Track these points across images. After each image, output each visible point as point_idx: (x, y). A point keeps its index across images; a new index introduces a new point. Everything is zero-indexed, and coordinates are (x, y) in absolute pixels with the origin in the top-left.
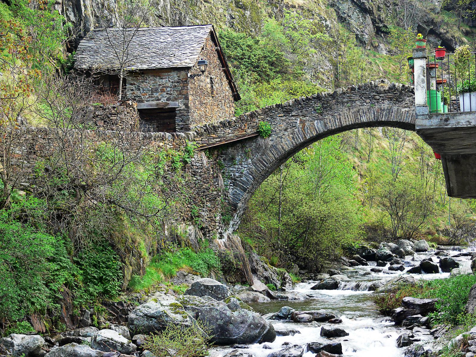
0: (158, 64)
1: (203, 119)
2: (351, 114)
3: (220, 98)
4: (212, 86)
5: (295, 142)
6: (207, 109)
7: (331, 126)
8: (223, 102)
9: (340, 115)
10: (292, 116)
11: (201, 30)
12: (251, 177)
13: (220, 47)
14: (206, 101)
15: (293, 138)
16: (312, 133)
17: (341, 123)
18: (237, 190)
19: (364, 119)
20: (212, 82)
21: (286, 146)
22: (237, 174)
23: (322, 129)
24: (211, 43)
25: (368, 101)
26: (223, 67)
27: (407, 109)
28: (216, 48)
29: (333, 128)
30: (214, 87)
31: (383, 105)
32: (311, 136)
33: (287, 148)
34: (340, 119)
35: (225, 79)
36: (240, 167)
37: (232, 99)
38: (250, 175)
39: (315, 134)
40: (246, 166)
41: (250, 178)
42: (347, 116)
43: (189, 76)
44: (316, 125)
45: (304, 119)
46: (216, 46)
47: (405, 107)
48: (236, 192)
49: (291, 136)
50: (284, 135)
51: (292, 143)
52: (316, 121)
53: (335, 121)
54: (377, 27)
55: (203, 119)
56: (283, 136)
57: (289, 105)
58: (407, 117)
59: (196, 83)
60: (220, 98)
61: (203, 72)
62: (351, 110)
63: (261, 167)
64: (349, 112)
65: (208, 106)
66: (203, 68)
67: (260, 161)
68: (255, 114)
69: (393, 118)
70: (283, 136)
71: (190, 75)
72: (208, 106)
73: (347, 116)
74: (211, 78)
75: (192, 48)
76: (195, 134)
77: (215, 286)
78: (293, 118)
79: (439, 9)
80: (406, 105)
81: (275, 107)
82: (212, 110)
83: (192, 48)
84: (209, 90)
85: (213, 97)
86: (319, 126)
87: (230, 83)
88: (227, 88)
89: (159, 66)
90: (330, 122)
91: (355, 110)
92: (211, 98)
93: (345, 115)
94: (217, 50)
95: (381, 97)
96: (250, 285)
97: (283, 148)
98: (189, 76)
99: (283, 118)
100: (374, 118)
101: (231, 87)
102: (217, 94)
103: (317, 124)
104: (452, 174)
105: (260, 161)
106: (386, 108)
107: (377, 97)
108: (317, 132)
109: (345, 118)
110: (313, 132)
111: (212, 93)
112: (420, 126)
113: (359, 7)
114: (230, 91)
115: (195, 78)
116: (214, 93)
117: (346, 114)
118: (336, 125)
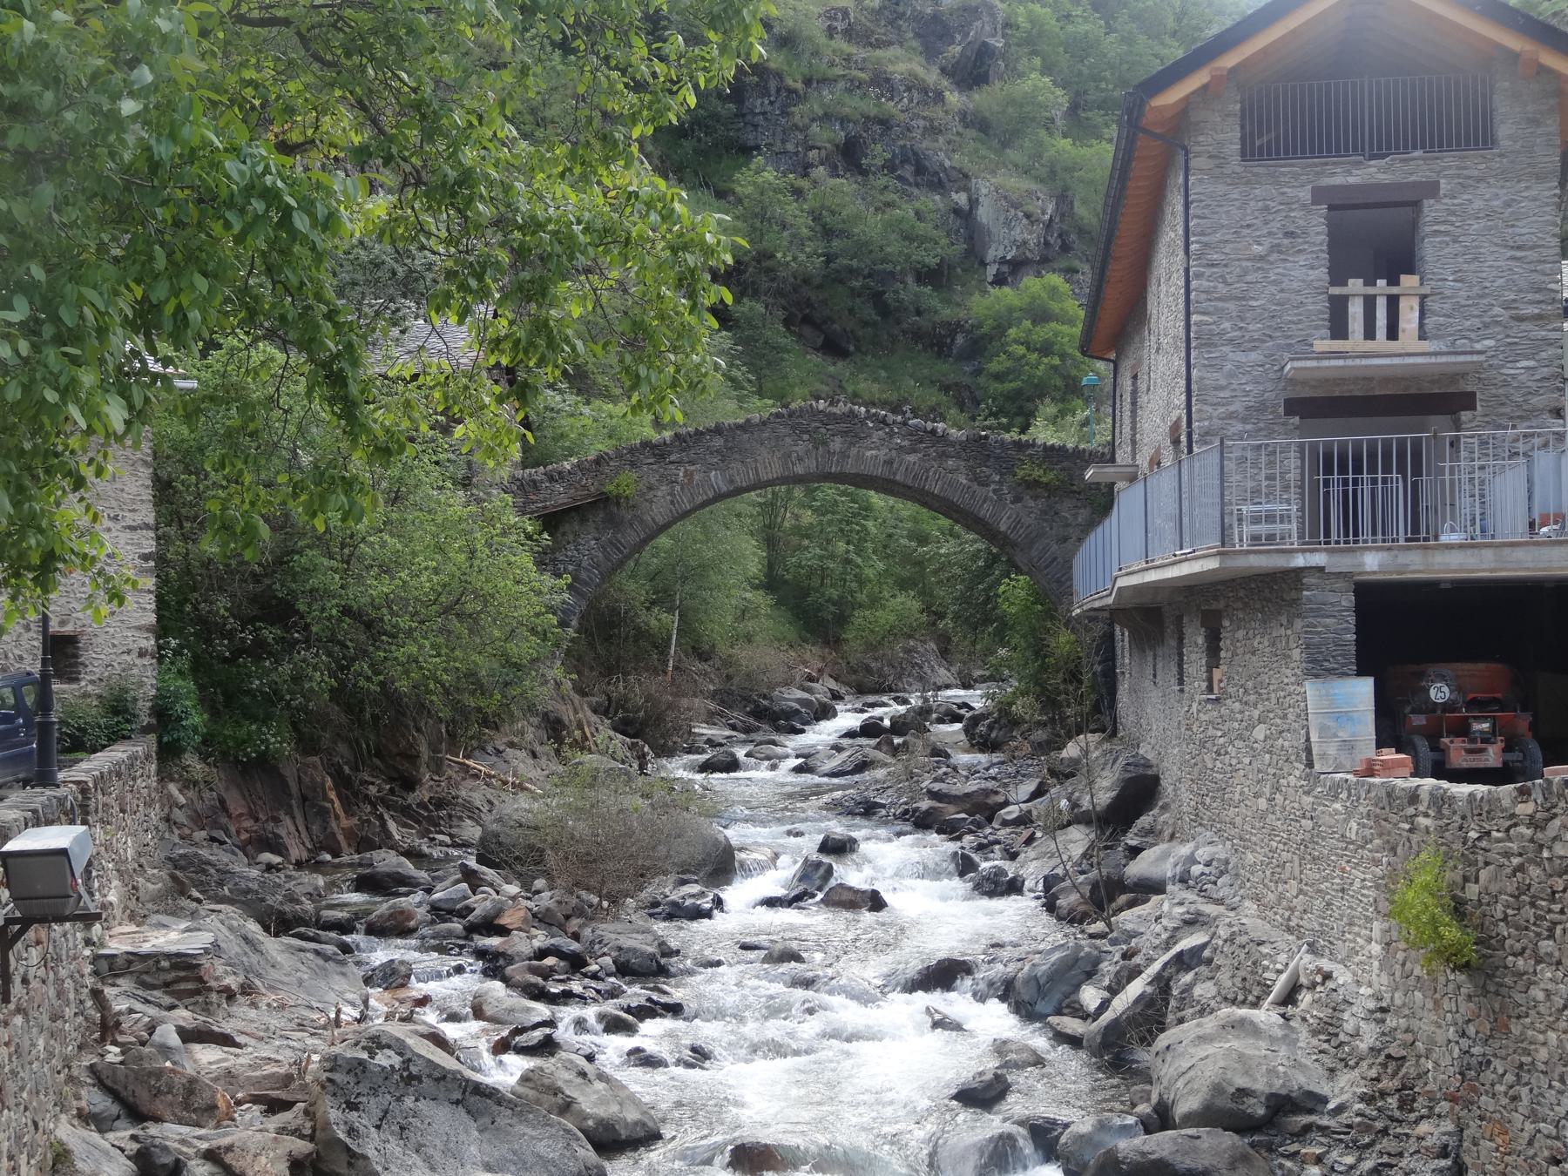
15: (672, 502)
25: (806, 437)
39: (711, 494)
69: (850, 467)
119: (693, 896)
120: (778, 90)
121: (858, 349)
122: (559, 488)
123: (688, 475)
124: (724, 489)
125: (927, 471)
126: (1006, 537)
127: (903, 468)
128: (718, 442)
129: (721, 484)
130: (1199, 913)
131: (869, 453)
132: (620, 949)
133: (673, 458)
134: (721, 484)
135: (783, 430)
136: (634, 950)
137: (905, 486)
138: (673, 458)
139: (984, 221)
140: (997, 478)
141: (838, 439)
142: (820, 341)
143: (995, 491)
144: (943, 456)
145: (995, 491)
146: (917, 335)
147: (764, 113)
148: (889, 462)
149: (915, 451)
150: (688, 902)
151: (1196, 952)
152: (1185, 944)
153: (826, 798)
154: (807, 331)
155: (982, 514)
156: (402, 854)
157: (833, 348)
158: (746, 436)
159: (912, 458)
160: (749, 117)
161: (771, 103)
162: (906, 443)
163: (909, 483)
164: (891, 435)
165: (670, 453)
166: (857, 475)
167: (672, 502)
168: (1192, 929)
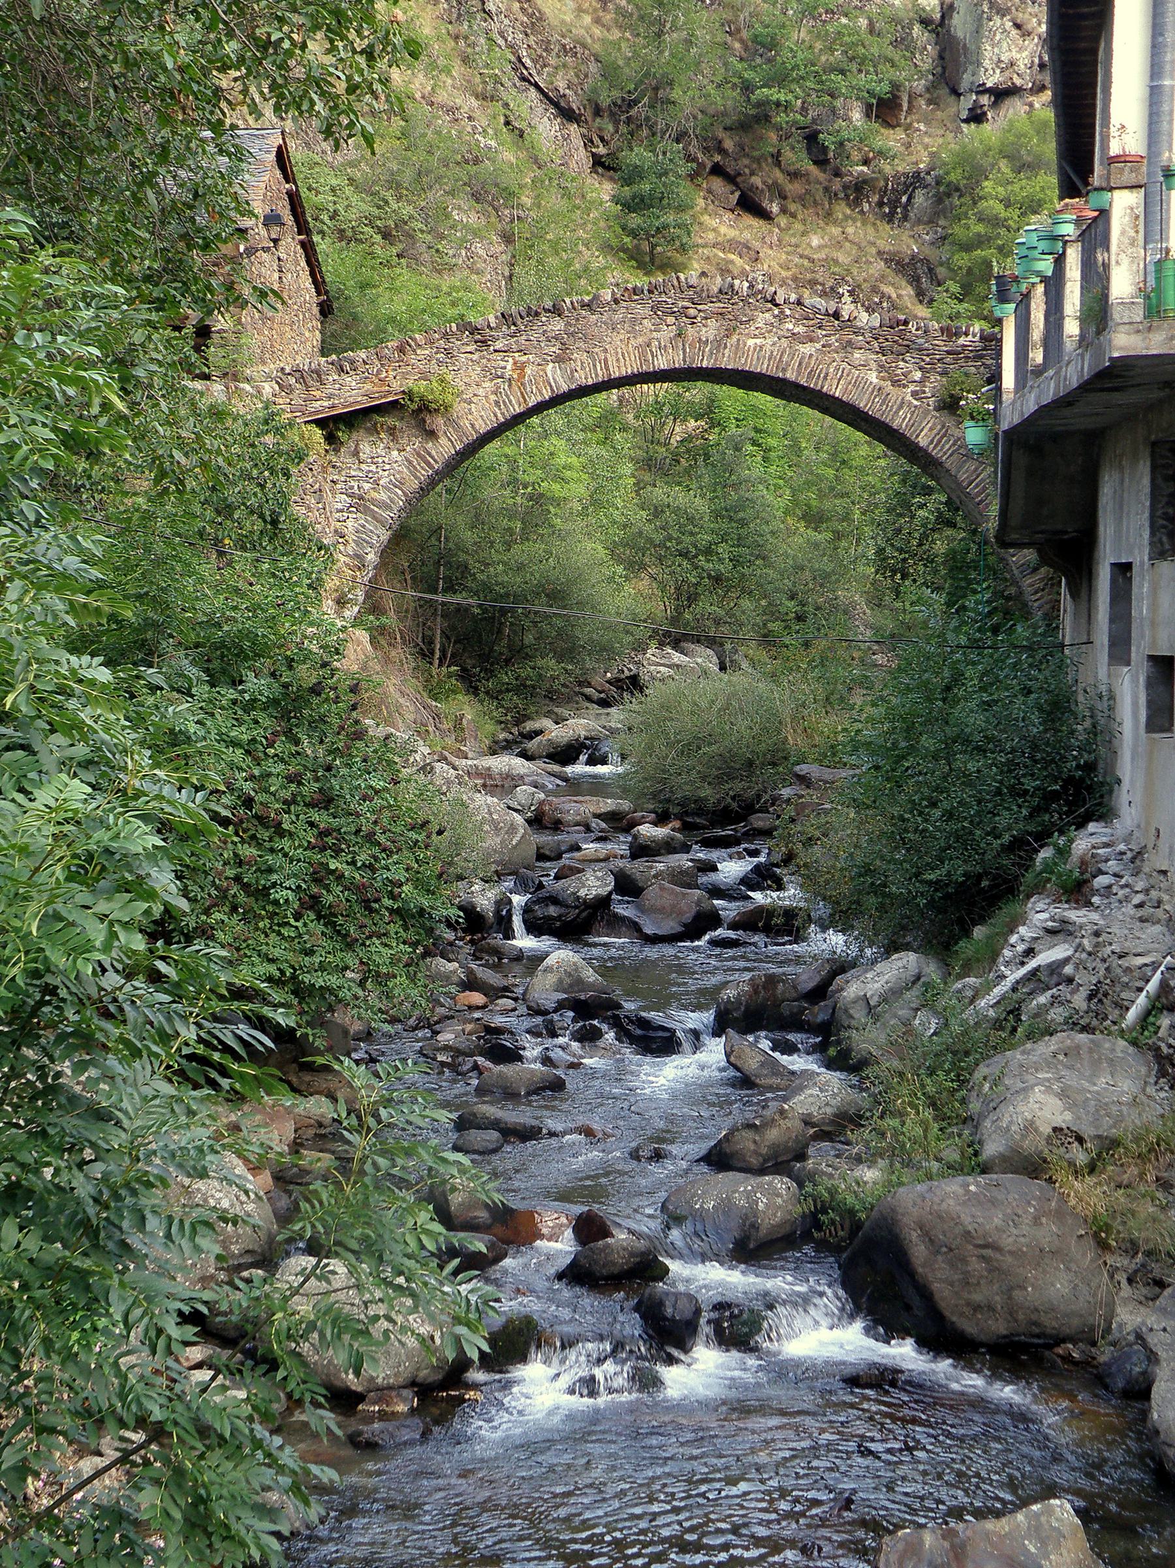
7: (585, 378)
9: (606, 351)
15: (497, 403)
17: (607, 369)
19: (662, 363)
22: (367, 486)
27: (758, 341)
29: (590, 382)
32: (540, 399)
34: (606, 360)
35: (303, 263)
36: (373, 468)
39: (547, 395)
41: (396, 494)
45: (524, 358)
47: (755, 337)
49: (493, 397)
54: (593, 155)
56: (475, 399)
62: (632, 341)
63: (424, 473)
67: (419, 455)
69: (727, 361)
70: (475, 399)
76: (277, 387)
78: (499, 356)
86: (558, 379)
87: (313, 274)
91: (640, 340)
97: (473, 425)
99: (475, 357)
101: (315, 282)
103: (554, 372)
104: (1018, 477)
105: (419, 455)
106: (711, 338)
107: (692, 312)
112: (1121, 348)
113: (556, 105)
121: (784, 210)
123: (520, 367)
124: (564, 388)
126: (924, 451)
127: (797, 360)
129: (561, 381)
130: (1064, 922)
131: (751, 342)
134: (561, 381)
137: (797, 386)
138: (499, 345)
139: (960, 34)
140: (918, 375)
141: (712, 323)
143: (914, 394)
144: (849, 346)
145: (914, 394)
146: (857, 191)
151: (1055, 968)
152: (1043, 958)
154: (717, 184)
155: (895, 425)
156: (762, 1171)
157: (750, 205)
159: (807, 349)
162: (800, 329)
163: (803, 382)
164: (782, 317)
166: (736, 372)
167: (497, 403)
168: (1056, 939)
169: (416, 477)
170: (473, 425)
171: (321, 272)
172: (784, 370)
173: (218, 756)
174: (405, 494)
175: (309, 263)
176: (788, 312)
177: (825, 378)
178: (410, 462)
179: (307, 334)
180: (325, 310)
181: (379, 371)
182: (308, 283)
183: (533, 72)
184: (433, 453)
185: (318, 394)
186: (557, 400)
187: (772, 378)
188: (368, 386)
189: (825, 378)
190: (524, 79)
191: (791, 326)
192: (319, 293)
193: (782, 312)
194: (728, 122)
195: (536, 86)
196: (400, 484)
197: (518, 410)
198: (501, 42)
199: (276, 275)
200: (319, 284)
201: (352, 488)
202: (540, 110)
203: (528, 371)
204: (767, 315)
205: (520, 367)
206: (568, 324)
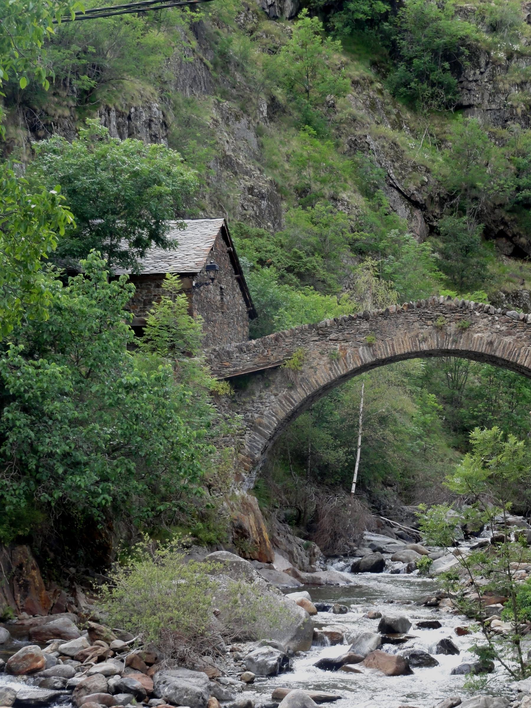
0: (152, 268)
1: (210, 341)
2: (406, 338)
3: (232, 314)
4: (222, 299)
5: (334, 375)
6: (216, 329)
7: (382, 355)
8: (236, 319)
9: (392, 339)
10: (331, 340)
11: (210, 225)
12: (275, 419)
13: (234, 249)
14: (214, 318)
16: (356, 363)
17: (394, 350)
18: (256, 435)
19: (425, 347)
20: (222, 294)
21: (321, 379)
22: (256, 415)
23: (369, 359)
24: (222, 242)
25: (429, 322)
26: (236, 274)
27: (480, 334)
28: (228, 249)
29: (384, 357)
30: (225, 299)
31: (449, 328)
32: (355, 366)
33: (323, 382)
34: (393, 345)
35: (238, 290)
37: (246, 316)
38: (273, 416)
39: (359, 364)
40: (269, 404)
41: (273, 420)
42: (402, 342)
43: (194, 285)
44: (361, 352)
46: (228, 246)
47: (478, 332)
48: (254, 438)
49: (329, 366)
50: (318, 364)
51: (330, 375)
52: (361, 348)
53: (386, 348)
55: (210, 341)
56: (318, 367)
57: (326, 326)
58: (480, 344)
59: (202, 294)
60: (232, 314)
61: (213, 279)
62: (408, 334)
63: (289, 408)
64: (405, 337)
65: (217, 325)
66: (212, 275)
68: (281, 337)
69: (462, 346)
71: (196, 284)
72: (217, 325)
73: (402, 342)
74: (221, 288)
75: (198, 249)
77: (236, 562)
79: (327, 197)
80: (479, 330)
81: (307, 328)
82: (222, 330)
83: (198, 249)
84: (218, 304)
85: (223, 313)
87: (244, 296)
88: (241, 302)
89: (155, 271)
90: (380, 349)
91: (413, 334)
92: (220, 314)
93: (399, 341)
94: (229, 252)
95: (446, 318)
96: (269, 562)
97: (317, 381)
98: (194, 285)
100: (438, 345)
102: (228, 309)
108: (362, 362)
109: (399, 345)
110: (358, 362)
111: (222, 307)
113: (409, 199)
114: (245, 305)
115: (202, 288)
116: (225, 307)
117: (400, 339)
118: (388, 353)
119: (264, 654)
120: (487, 64)
122: (247, 357)
123: (343, 349)
125: (520, 349)
127: (501, 347)
128: (365, 326)
129: (367, 356)
131: (476, 336)
132: (176, 688)
133: (332, 336)
134: (367, 356)
135: (412, 318)
136: (187, 690)
138: (332, 336)
142: (510, 250)
147: (476, 81)
148: (491, 343)
149: (510, 334)
150: (260, 659)
153: (89, 658)
158: (386, 322)
159: (508, 339)
160: (465, 83)
161: (482, 73)
162: (504, 328)
164: (493, 322)
165: (331, 333)
167: (331, 369)
169: (284, 410)
170: (317, 381)
171: (249, 294)
172: (495, 351)
173: (498, 442)
174: (277, 419)
175: (242, 289)
176: (497, 318)
177: (518, 356)
178: (281, 402)
179: (239, 329)
180: (252, 314)
181: (263, 351)
182: (241, 301)
183: (396, 182)
184: (295, 397)
185: (227, 364)
186: (366, 367)
187: (489, 355)
188: (257, 360)
189: (518, 356)
190: (391, 185)
191: (498, 326)
192: (248, 306)
193: (494, 319)
194: (507, 208)
195: (397, 189)
196: (276, 414)
197: (343, 372)
198: (378, 165)
199: (219, 298)
200: (248, 301)
201: (248, 416)
202: (399, 201)
203: (349, 351)
204: (485, 320)
205: (343, 349)
206: (371, 325)
